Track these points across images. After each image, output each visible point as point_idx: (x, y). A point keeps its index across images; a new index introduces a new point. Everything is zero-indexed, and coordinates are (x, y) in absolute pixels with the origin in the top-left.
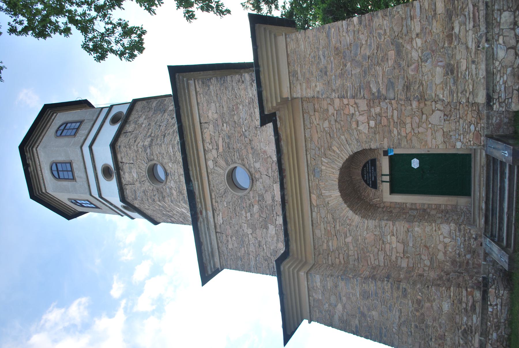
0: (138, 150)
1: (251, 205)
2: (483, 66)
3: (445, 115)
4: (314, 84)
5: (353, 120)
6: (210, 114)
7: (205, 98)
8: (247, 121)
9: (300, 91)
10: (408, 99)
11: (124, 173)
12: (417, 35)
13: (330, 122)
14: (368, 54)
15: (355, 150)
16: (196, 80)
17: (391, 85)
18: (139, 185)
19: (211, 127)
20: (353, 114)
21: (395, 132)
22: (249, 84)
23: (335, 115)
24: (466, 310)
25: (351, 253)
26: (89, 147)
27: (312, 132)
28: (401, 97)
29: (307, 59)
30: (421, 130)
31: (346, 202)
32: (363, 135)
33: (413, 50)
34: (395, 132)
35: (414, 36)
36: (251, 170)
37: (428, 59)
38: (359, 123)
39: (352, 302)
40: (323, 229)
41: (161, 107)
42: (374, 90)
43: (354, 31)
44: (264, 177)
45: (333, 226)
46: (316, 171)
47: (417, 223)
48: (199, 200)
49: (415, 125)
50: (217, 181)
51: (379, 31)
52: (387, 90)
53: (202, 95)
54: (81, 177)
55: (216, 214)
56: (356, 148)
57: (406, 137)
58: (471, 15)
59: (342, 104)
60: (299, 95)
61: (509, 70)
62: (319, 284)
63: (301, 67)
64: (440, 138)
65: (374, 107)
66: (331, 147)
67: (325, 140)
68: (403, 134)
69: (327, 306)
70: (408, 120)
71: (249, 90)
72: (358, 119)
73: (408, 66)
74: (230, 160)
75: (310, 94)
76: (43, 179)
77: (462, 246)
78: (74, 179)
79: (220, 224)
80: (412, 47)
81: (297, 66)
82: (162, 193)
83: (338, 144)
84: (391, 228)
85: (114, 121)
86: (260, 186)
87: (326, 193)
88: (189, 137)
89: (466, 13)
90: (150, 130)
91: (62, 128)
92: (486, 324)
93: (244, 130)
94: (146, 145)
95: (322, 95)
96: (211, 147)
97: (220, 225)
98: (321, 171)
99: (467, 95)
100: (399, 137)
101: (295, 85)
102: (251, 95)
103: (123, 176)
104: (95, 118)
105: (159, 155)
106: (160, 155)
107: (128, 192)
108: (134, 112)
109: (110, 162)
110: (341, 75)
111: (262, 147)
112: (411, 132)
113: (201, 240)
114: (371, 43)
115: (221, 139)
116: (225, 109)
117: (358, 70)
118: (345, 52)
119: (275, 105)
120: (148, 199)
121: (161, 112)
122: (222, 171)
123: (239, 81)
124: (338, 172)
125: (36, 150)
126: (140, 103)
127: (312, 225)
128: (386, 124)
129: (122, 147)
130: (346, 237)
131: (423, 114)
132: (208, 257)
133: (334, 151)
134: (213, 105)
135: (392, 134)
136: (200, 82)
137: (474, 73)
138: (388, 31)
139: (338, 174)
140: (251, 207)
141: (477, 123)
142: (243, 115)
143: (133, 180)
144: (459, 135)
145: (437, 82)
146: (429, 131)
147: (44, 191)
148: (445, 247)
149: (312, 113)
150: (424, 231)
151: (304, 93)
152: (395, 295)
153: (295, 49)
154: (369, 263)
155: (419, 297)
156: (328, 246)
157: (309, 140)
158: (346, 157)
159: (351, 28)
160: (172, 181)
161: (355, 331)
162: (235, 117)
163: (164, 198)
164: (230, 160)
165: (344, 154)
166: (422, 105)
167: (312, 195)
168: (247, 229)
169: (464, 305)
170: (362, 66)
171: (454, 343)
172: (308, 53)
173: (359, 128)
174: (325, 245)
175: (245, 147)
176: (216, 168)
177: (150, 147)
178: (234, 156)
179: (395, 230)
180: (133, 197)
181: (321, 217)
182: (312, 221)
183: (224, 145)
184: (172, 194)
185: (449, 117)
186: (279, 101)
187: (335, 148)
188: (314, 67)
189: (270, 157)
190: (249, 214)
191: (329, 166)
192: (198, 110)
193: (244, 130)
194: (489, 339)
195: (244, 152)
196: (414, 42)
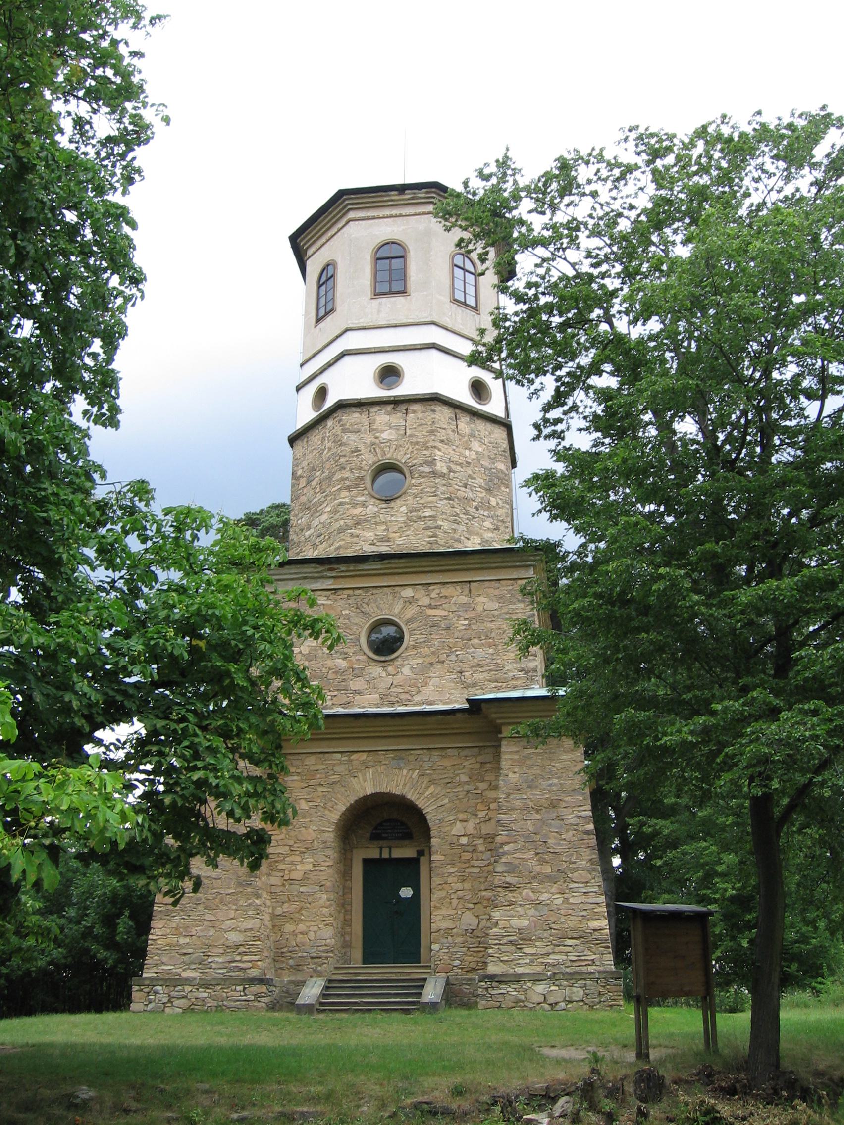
0: (427, 448)
2: (527, 971)
3: (473, 930)
4: (516, 770)
6: (482, 599)
11: (389, 414)
13: (467, 783)
14: (550, 841)
15: (428, 817)
19: (464, 599)
21: (452, 870)
30: (455, 902)
31: (356, 801)
34: (452, 870)
35: (566, 896)
40: (317, 767)
41: (496, 481)
42: (506, 848)
43: (577, 825)
48: (351, 568)
51: (575, 856)
53: (510, 588)
54: (379, 312)
55: (329, 593)
56: (432, 818)
57: (446, 883)
58: (583, 958)
60: (503, 749)
61: (522, 997)
64: (444, 925)
68: (450, 880)
70: (467, 885)
74: (414, 626)
75: (505, 764)
80: (553, 894)
83: (437, 794)
84: (323, 863)
90: (458, 468)
98: (400, 769)
107: (353, 417)
108: (489, 426)
114: (562, 845)
115: (446, 613)
116: (489, 625)
121: (486, 484)
122: (396, 611)
124: (398, 793)
125: (429, 213)
126: (504, 435)
128: (463, 858)
130: (308, 801)
131: (475, 904)
133: (427, 788)
137: (520, 961)
139: (397, 793)
140: (343, 656)
141: (462, 968)
146: (454, 912)
147: (351, 215)
148: (301, 933)
150: (323, 907)
151: (507, 756)
158: (420, 804)
162: (476, 641)
166: (485, 903)
167: (365, 754)
169: (238, 958)
175: (433, 653)
176: (401, 601)
178: (421, 634)
181: (334, 765)
184: (355, 505)
186: (498, 721)
187: (432, 789)
189: (419, 692)
195: (425, 651)
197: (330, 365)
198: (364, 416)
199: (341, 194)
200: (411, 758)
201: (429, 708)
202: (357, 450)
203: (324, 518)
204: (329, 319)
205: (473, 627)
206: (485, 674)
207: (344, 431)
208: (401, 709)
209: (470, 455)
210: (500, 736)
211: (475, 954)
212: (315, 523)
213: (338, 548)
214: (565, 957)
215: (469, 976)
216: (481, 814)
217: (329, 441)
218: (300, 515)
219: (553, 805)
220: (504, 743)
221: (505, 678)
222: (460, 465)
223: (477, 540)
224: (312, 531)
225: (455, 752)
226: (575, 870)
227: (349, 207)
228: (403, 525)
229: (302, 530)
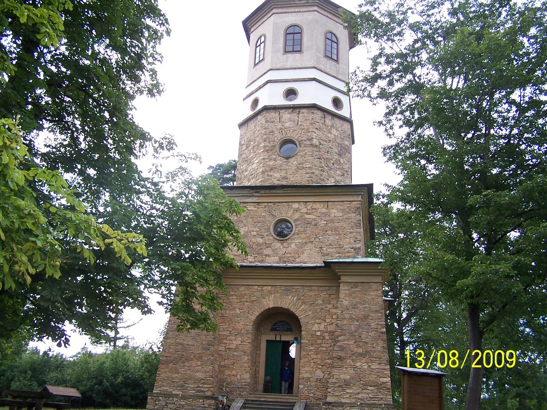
0: (309, 132)
1: (262, 237)
2: (347, 401)
3: (321, 379)
4: (347, 299)
6: (334, 211)
10: (332, 358)
11: (290, 113)
12: (370, 366)
14: (362, 336)
16: (360, 202)
17: (342, 348)
19: (324, 210)
20: (326, 321)
21: (312, 348)
22: (354, 246)
25: (228, 312)
26: (315, 78)
30: (312, 364)
33: (361, 363)
34: (312, 348)
35: (369, 364)
36: (290, 240)
38: (320, 325)
42: (340, 338)
43: (377, 329)
44: (284, 250)
45: (248, 300)
47: (250, 358)
48: (267, 192)
49: (315, 360)
52: (339, 346)
53: (349, 205)
54: (287, 61)
55: (255, 204)
57: (308, 355)
58: (376, 397)
59: (333, 314)
63: (359, 291)
67: (310, 300)
70: (319, 356)
71: (349, 246)
73: (352, 360)
74: (298, 223)
75: (342, 295)
76: (286, 13)
77: (235, 386)
78: (286, 52)
79: (247, 207)
84: (246, 341)
85: (337, 102)
87: (272, 297)
88: (318, 191)
89: (378, 394)
90: (325, 143)
91: (334, 39)
92: (190, 398)
93: (320, 238)
94: (313, 141)
95: (340, 304)
96: (309, 208)
97: (246, 207)
99: (333, 392)
102: (345, 247)
103: (287, 112)
104: (340, 77)
105: (304, 152)
106: (304, 154)
109: (298, 101)
110: (351, 318)
111: (307, 251)
112: (311, 358)
113: (234, 190)
115: (315, 217)
116: (337, 224)
119: (337, 271)
120: (266, 134)
121: (339, 152)
122: (289, 215)
123: (356, 238)
125: (315, 11)
126: (349, 127)
127: (248, 285)
129: (313, 116)
131: (322, 366)
133: (301, 306)
134: (341, 214)
135: (310, 346)
136: (359, 206)
138: (374, 349)
142: (331, 238)
143: (283, 121)
144: (307, 387)
147: (274, 11)
149: (328, 292)
150: (245, 363)
152: (204, 343)
153: (372, 288)
154: (220, 324)
155: (204, 358)
156: (232, 295)
158: (297, 313)
159: (379, 327)
162: (330, 232)
163: (267, 151)
164: (298, 223)
166: (328, 366)
167: (270, 287)
168: (244, 231)
169: (201, 386)
170: (355, 332)
171: (174, 379)
174: (233, 293)
175: (307, 237)
176: (292, 210)
177: (311, 144)
179: (245, 344)
180: (268, 119)
181: (254, 292)
182: (251, 285)
186: (339, 274)
188: (358, 300)
190: (255, 233)
192: (338, 201)
193: (320, 238)
194: (180, 400)
195: (303, 236)
196: (366, 364)
197: (260, 88)
198: (277, 114)
201: (304, 265)
202: (273, 132)
205: (328, 225)
206: (334, 249)
208: (290, 265)
209: (331, 136)
211: (321, 391)
212: (250, 168)
214: (367, 396)
215: (318, 402)
219: (366, 317)
221: (344, 252)
222: (326, 141)
223: (333, 180)
224: (248, 172)
225: (316, 288)
226: (375, 351)
227: (273, 7)
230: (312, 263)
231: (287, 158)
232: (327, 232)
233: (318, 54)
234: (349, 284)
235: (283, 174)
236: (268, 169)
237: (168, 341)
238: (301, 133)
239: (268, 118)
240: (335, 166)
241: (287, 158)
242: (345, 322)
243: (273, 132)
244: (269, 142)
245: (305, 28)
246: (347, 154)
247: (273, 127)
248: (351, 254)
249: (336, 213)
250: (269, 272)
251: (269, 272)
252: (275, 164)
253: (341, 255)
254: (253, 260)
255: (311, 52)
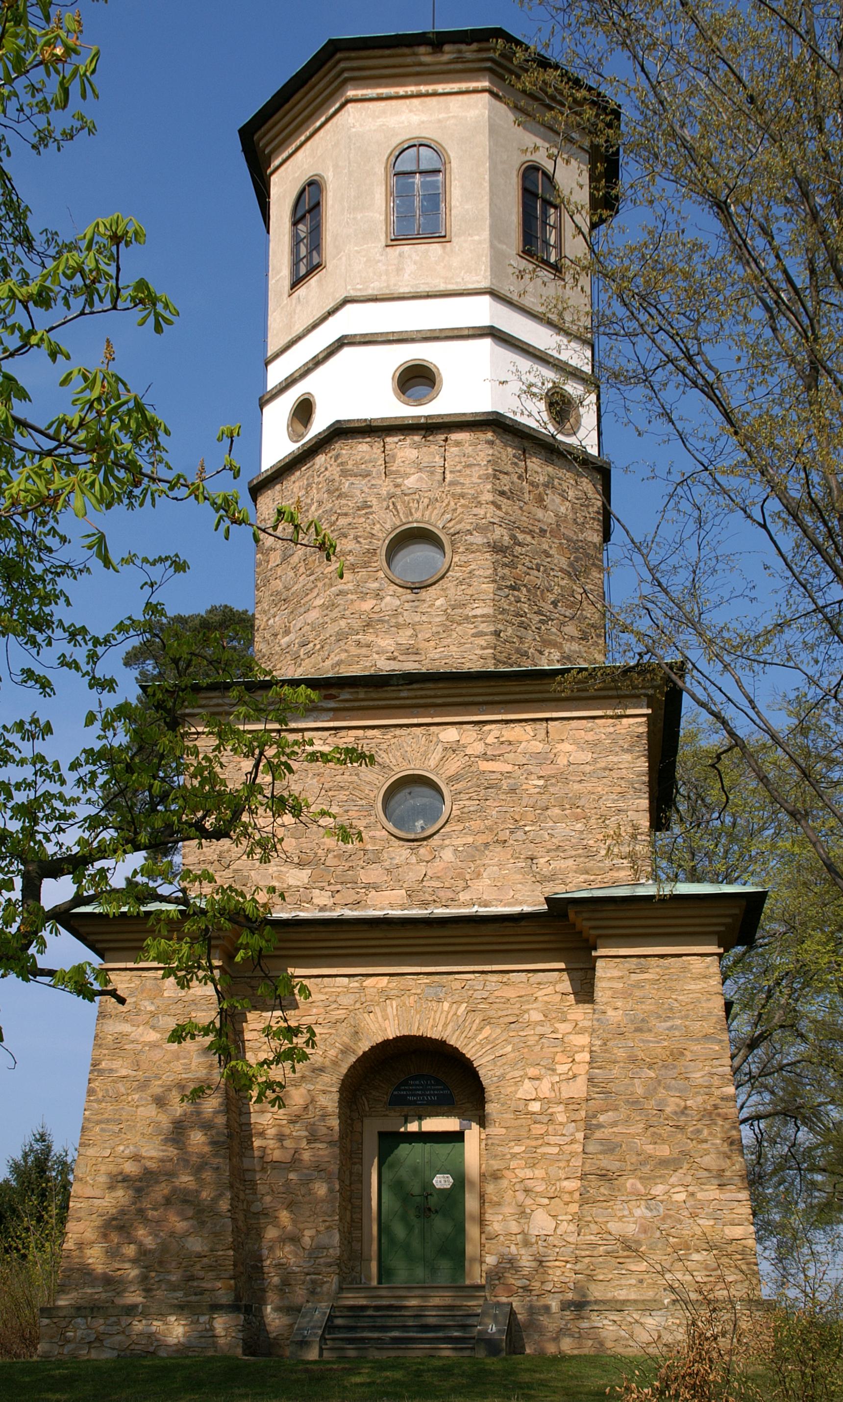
2: (633, 1296)
4: (619, 1004)
5: (543, 1071)
6: (566, 747)
7: (604, 737)
8: (547, 837)
9: (609, 975)
11: (418, 447)
12: (692, 1194)
13: (540, 1023)
15: (481, 1072)
17: (610, 1147)
18: (384, 492)
20: (554, 1070)
21: (517, 1149)
23: (554, 1036)
24: (192, 1278)
27: (521, 985)
28: (587, 1165)
29: (668, 994)
32: (513, 1089)
34: (517, 1149)
35: (690, 1189)
37: (651, 1210)
38: (537, 1082)
39: (168, 1062)
42: (602, 1118)
44: (422, 868)
45: (320, 1021)
46: (439, 989)
48: (362, 696)
50: (409, 749)
53: (611, 730)
54: (399, 270)
56: (486, 1074)
62: (199, 993)
65: (566, 1111)
66: (489, 1023)
67: (505, 1013)
68: (513, 1164)
69: (149, 1008)
70: (539, 1173)
72: (545, 1080)
73: (640, 1178)
78: (396, 240)
80: (673, 1186)
81: (658, 974)
82: (366, 565)
83: (495, 1039)
86: (401, 856)
88: (517, 689)
90: (529, 539)
93: (527, 829)
96: (490, 739)
100: (509, 1156)
101: (621, 966)
110: (633, 1059)
112: (517, 1177)
115: (509, 768)
116: (576, 786)
117: (640, 1091)
118: (675, 1067)
121: (571, 565)
122: (432, 763)
125: (483, 91)
128: (534, 1132)
132: (215, 701)
134: (588, 756)
135: (513, 1143)
137: (623, 1282)
139: (434, 1037)
142: (562, 829)
143: (397, 472)
145: (609, 1225)
147: (351, 93)
153: (690, 970)
157: (505, 980)
159: (716, 1081)
160: (398, 603)
161: (100, 1067)
162: (557, 811)
165: (474, 1050)
172: (680, 998)
173: (527, 1080)
175: (490, 829)
176: (440, 748)
178: (470, 799)
183: (494, 776)
184: (363, 596)
185: (545, 1244)
187: (487, 1031)
191: (449, 1017)
193: (527, 829)
195: (477, 824)
196: (681, 1189)
197: (317, 362)
198: (378, 446)
199: (334, 48)
200: (457, 985)
201: (483, 911)
202: (366, 506)
203: (313, 615)
204: (314, 281)
205: (552, 790)
206: (570, 862)
207: (345, 473)
208: (440, 911)
209: (549, 517)
210: (594, 954)
212: (299, 622)
213: (339, 663)
216: (561, 1069)
217: (318, 490)
218: (272, 611)
219: (677, 1055)
220: (600, 964)
221: (600, 868)
222: (531, 532)
223: (556, 655)
224: (292, 636)
227: (346, 75)
228: (440, 629)
229: (275, 635)
230: (505, 906)
231: (415, 588)
232: (549, 812)
233: (500, 246)
234: (621, 963)
235: (404, 637)
236: (356, 624)
237: (91, 1152)
238: (455, 510)
239: (350, 462)
240: (561, 609)
241: (415, 588)
242: (616, 1071)
243: (366, 506)
244: (356, 538)
245: (453, 153)
246: (595, 574)
247: (367, 490)
248: (622, 874)
249: (574, 754)
250: (381, 935)
251: (381, 935)
252: (377, 609)
253: (592, 878)
254: (329, 902)
255: (476, 238)
